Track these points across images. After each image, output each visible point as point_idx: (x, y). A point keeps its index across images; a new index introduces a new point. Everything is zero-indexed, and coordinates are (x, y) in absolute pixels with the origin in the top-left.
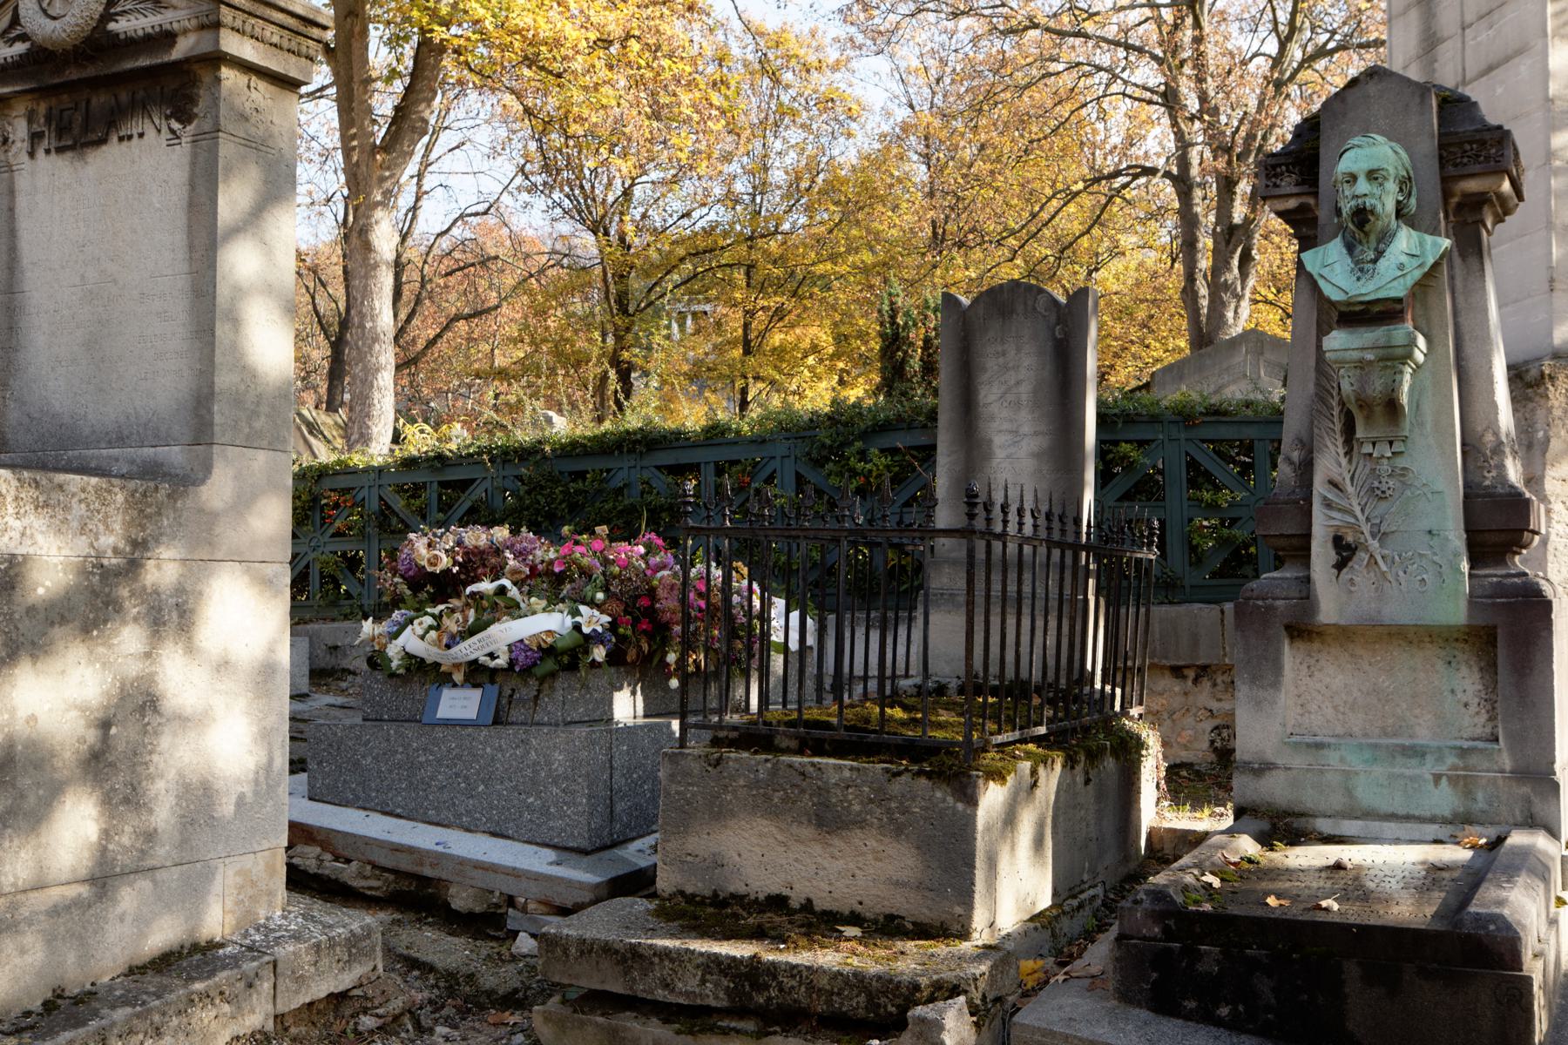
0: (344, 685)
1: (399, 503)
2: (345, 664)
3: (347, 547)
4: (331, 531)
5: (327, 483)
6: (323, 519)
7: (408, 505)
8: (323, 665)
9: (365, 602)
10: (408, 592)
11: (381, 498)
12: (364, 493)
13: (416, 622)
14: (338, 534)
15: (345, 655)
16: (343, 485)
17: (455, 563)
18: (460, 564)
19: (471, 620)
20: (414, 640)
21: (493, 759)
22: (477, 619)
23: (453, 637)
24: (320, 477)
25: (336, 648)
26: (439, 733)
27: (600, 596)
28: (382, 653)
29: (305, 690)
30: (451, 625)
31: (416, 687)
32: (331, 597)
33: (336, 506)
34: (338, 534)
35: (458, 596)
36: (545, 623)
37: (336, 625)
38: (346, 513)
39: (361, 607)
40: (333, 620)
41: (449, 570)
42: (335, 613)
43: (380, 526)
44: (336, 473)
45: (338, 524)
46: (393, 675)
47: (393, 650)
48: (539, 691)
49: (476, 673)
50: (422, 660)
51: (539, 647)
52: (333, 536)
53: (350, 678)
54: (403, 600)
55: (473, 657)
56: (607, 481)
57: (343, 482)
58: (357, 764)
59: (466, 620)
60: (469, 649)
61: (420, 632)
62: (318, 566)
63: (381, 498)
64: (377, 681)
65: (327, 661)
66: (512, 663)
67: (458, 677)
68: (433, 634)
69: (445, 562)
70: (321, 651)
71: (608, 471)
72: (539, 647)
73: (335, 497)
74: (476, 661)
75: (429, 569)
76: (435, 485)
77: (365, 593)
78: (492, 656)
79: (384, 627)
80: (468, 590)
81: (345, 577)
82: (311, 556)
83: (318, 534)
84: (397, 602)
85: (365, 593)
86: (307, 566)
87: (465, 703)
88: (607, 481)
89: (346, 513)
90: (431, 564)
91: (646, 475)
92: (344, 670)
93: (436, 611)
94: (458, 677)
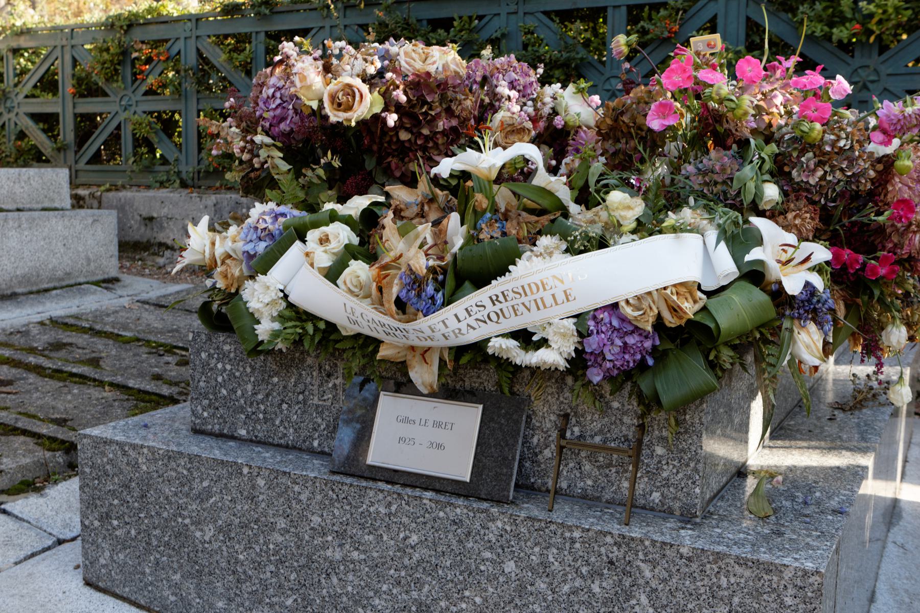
0: (161, 261)
1: (219, 58)
2: (161, 237)
3: (161, 107)
4: (144, 88)
5: (138, 34)
6: (134, 74)
7: (231, 59)
8: (137, 237)
9: (183, 168)
10: (285, 166)
11: (199, 53)
12: (180, 45)
13: (313, 235)
14: (150, 92)
15: (162, 228)
16: (156, 37)
17: (390, 104)
18: (398, 108)
19: (458, 242)
20: (308, 278)
21: (521, 589)
22: (472, 239)
23: (415, 282)
24: (130, 26)
25: (151, 219)
26: (378, 500)
27: (772, 192)
28: (232, 296)
29: (114, 273)
30: (409, 249)
31: (312, 379)
32: (145, 163)
33: (149, 60)
34: (150, 92)
35: (411, 182)
36: (666, 263)
37: (151, 193)
38: (158, 70)
39: (179, 173)
40: (148, 187)
41: (377, 119)
42: (150, 179)
43: (199, 83)
44: (148, 23)
45: (151, 80)
46: (257, 349)
47: (259, 296)
48: (642, 428)
49: (468, 371)
50: (332, 327)
51: (659, 323)
52: (146, 93)
53: (168, 253)
54: (273, 184)
55: (472, 337)
56: (478, 30)
57: (155, 33)
58: (182, 534)
59: (441, 240)
60: (464, 320)
61: (324, 260)
62: (130, 127)
63: (199, 53)
64: (223, 356)
65: (139, 233)
66: (579, 362)
67: (424, 375)
68: (358, 269)
69: (369, 104)
70: (134, 222)
71: (480, 18)
72: (659, 323)
73: (146, 49)
74: (479, 347)
75: (334, 117)
76: (262, 36)
77: (182, 158)
78: (524, 337)
79: (233, 240)
80: (446, 167)
81: (160, 141)
82: (122, 117)
83: (129, 92)
84: (258, 185)
85: (182, 158)
86: (118, 127)
87: (439, 435)
88: (478, 30)
89: (158, 70)
90: (338, 106)
91: (531, 23)
92: (161, 245)
93: (358, 204)
94: (424, 375)
